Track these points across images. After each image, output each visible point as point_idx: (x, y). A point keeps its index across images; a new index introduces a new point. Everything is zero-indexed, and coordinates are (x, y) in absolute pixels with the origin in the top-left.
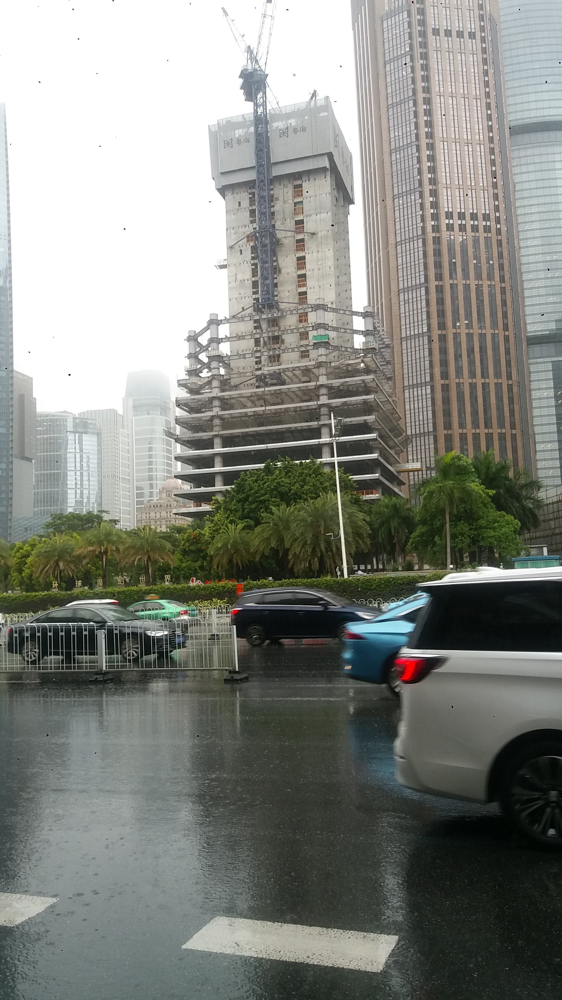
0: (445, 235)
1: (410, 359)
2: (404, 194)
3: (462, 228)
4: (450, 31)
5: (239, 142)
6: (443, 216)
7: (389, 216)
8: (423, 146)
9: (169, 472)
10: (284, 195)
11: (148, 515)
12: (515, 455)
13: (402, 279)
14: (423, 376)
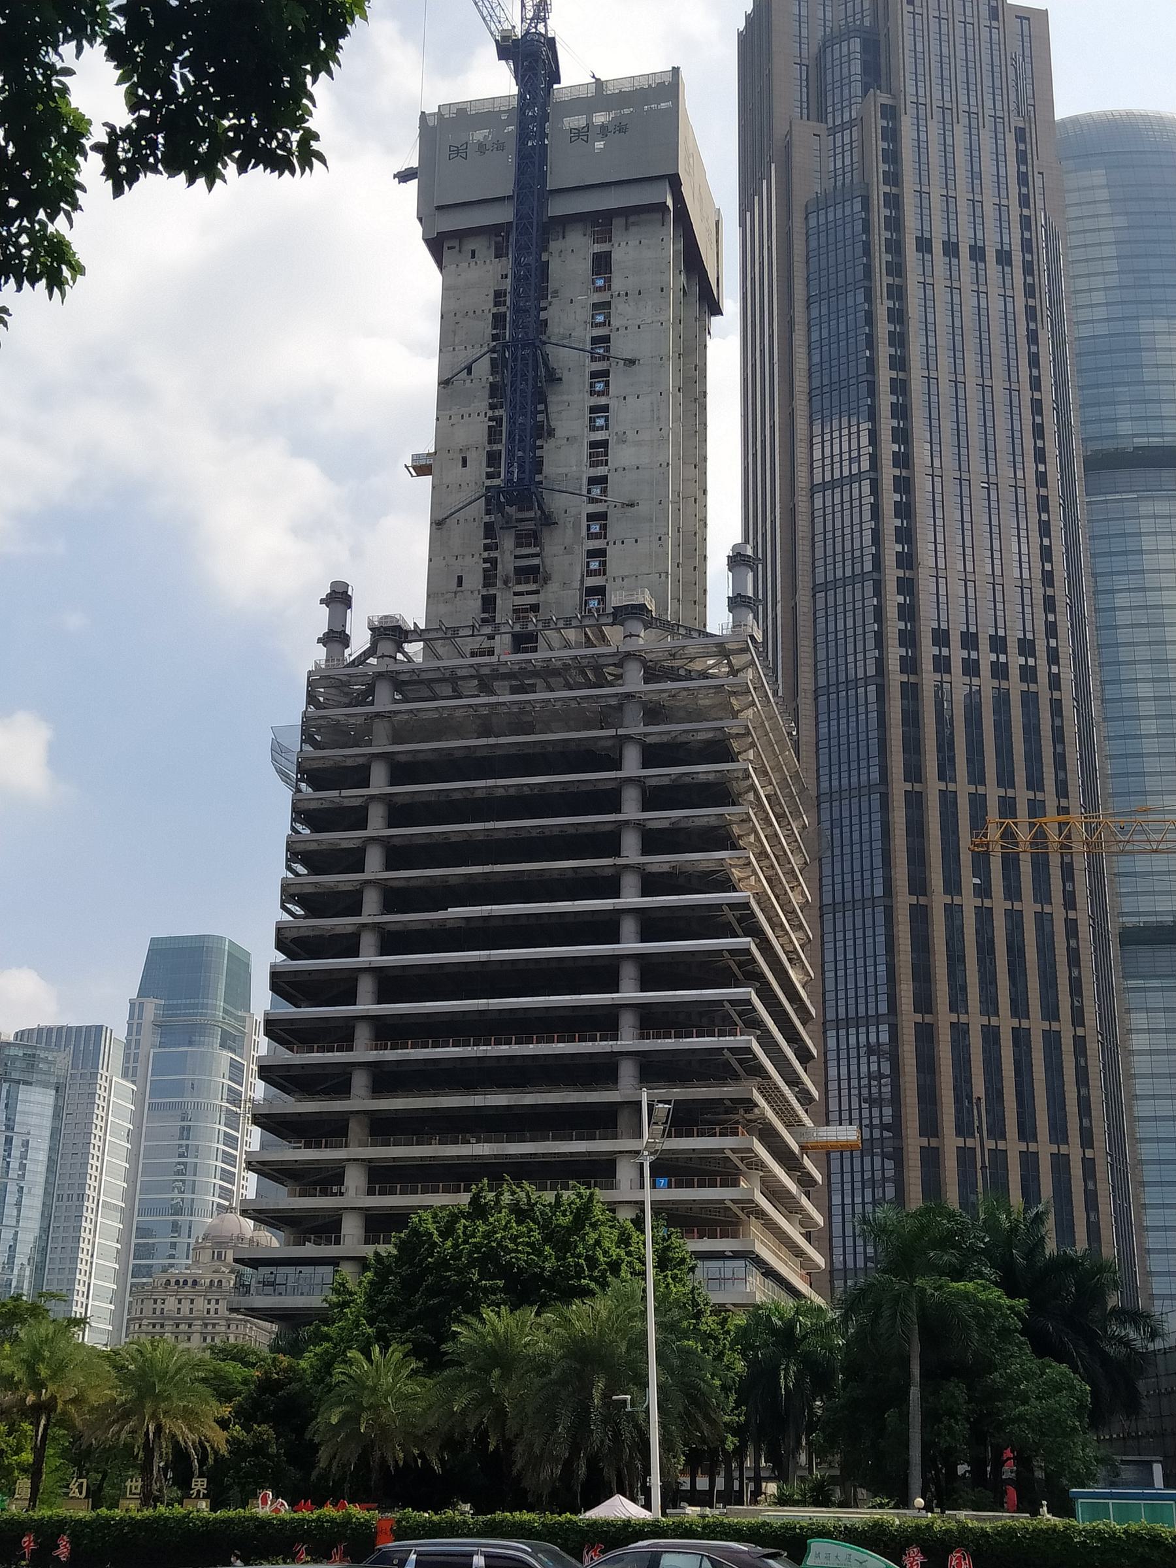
0: (929, 678)
1: (841, 987)
2: (840, 583)
4: (975, 635)
5: (482, 148)
7: (796, 251)
8: (887, 483)
9: (226, 1193)
10: (570, 259)
11: (159, 1306)
12: (1083, 1091)
13: (822, 613)
14: (871, 999)
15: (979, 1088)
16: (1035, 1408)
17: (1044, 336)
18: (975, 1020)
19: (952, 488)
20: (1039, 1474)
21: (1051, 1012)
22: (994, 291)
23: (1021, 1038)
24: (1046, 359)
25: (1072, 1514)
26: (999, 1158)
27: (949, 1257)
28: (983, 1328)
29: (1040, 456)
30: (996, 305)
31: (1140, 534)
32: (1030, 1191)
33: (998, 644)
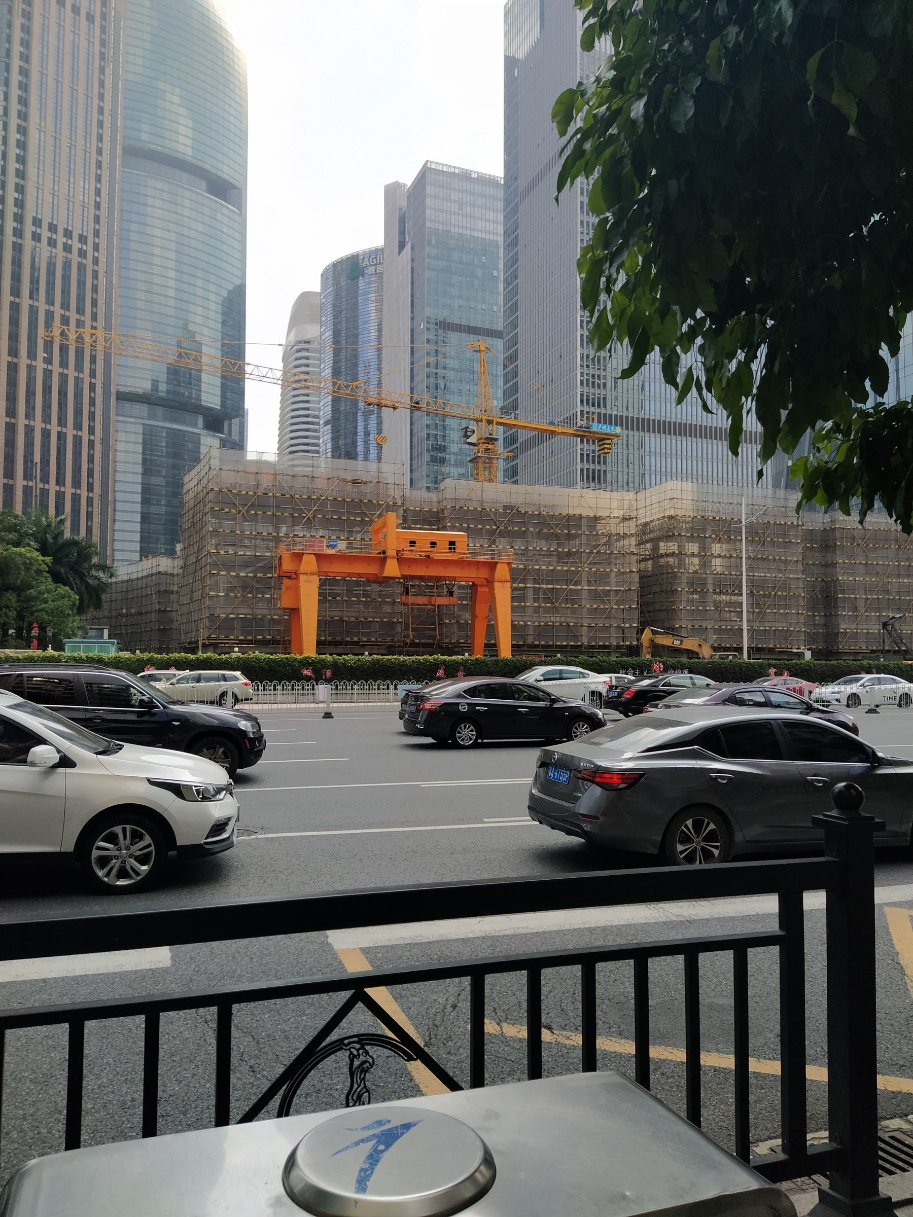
0: (28, 243)
3: (52, 243)
6: (28, 222)
15: (37, 458)
16: (51, 605)
17: (109, 71)
18: (38, 425)
19: (50, 141)
20: (50, 634)
21: (78, 426)
22: (83, 36)
23: (61, 436)
24: (108, 84)
25: (64, 650)
26: (45, 493)
27: (12, 536)
28: (28, 569)
29: (100, 138)
30: (84, 44)
31: (147, 195)
32: (59, 509)
33: (68, 234)
